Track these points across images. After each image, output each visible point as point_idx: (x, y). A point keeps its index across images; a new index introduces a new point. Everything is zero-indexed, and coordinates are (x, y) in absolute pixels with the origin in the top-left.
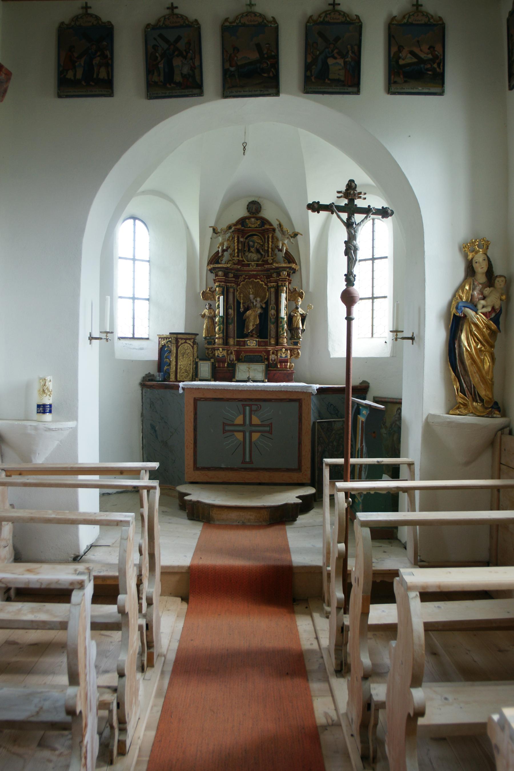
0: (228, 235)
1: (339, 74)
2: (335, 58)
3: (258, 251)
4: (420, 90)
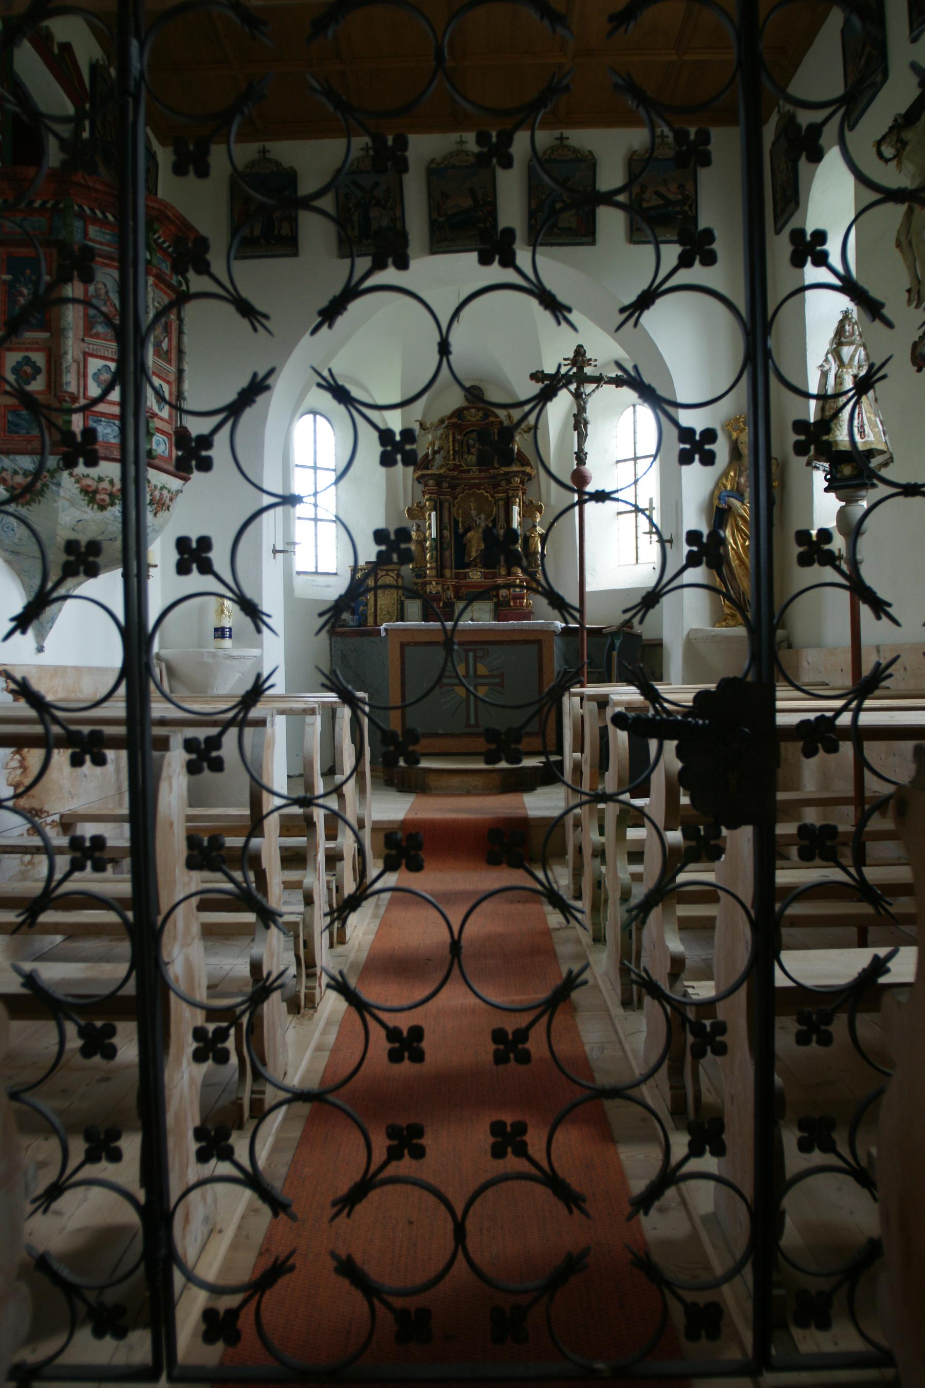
0: (440, 432)
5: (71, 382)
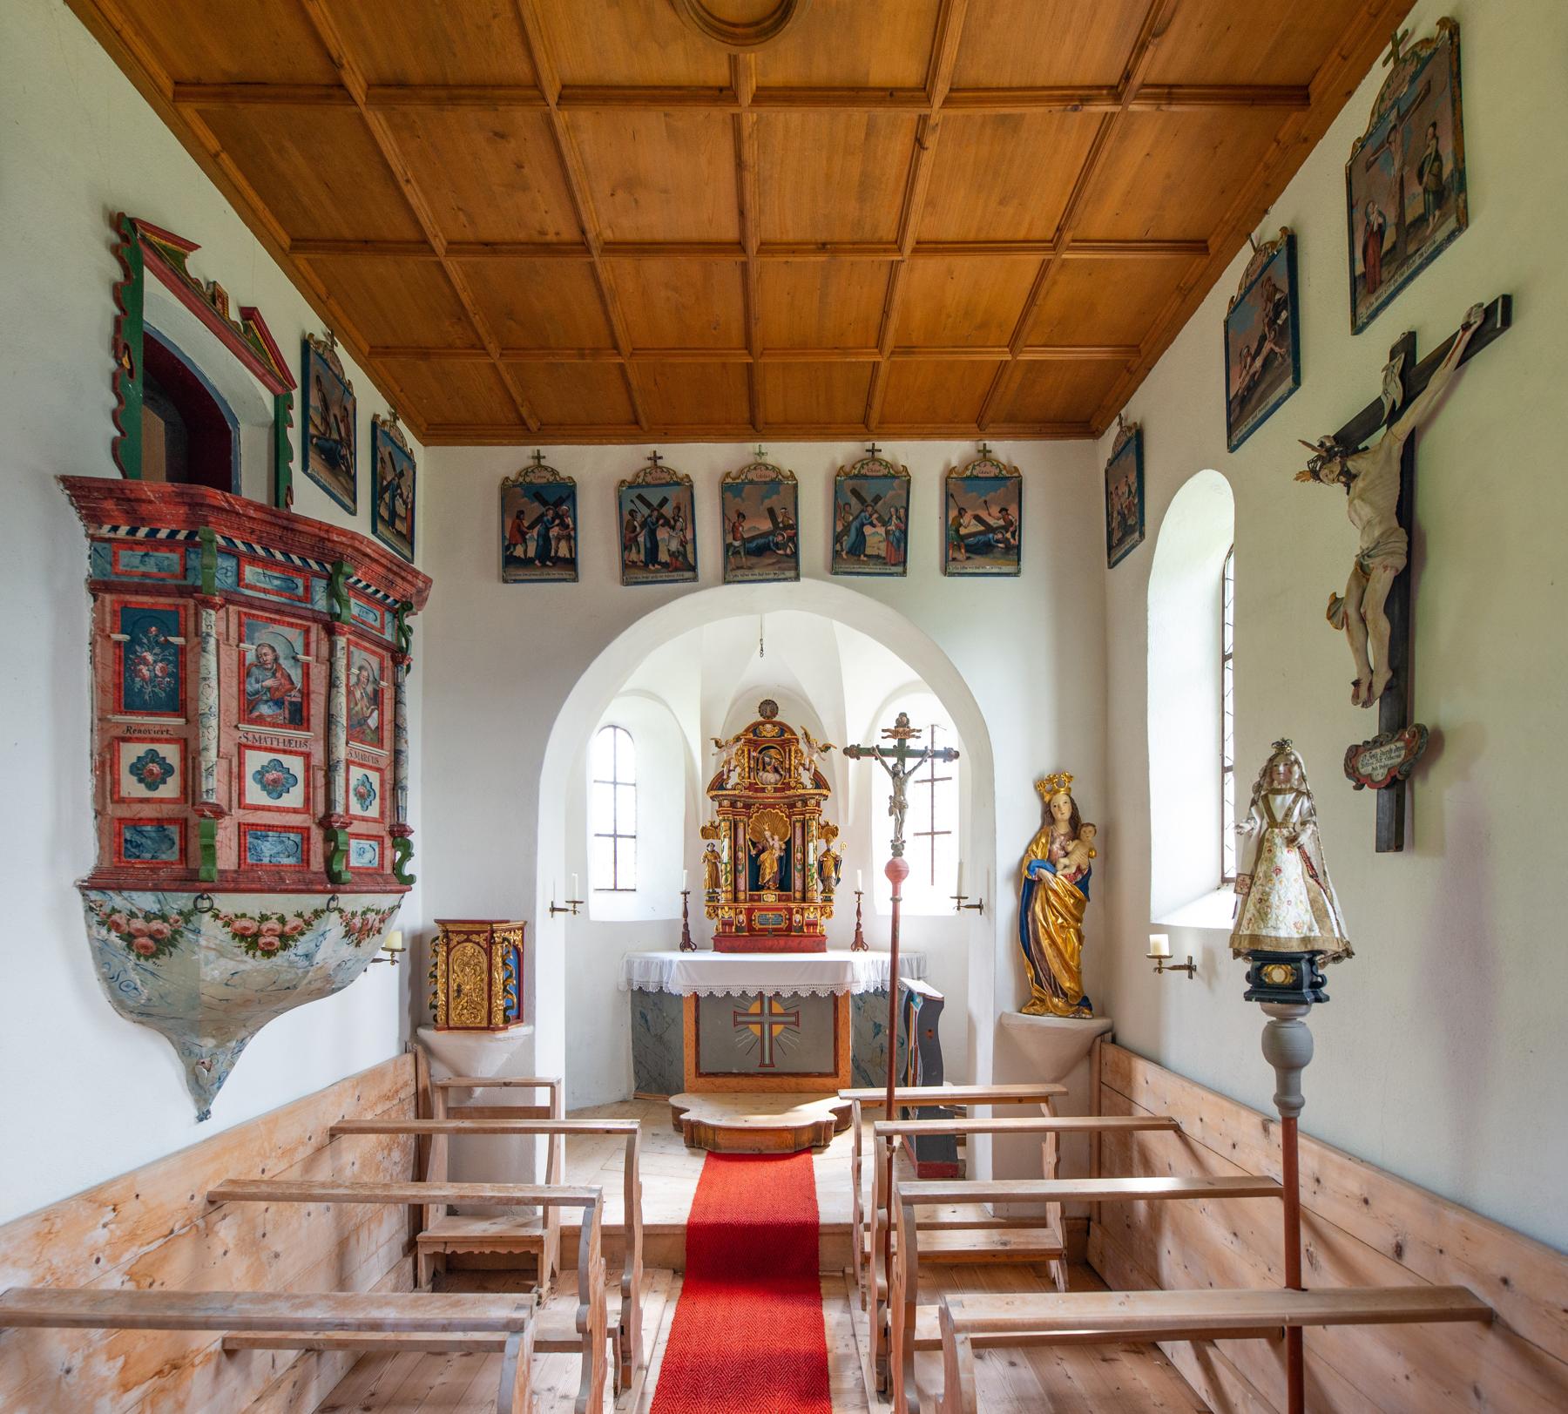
3: (776, 770)
4: (988, 569)
5: (214, 787)
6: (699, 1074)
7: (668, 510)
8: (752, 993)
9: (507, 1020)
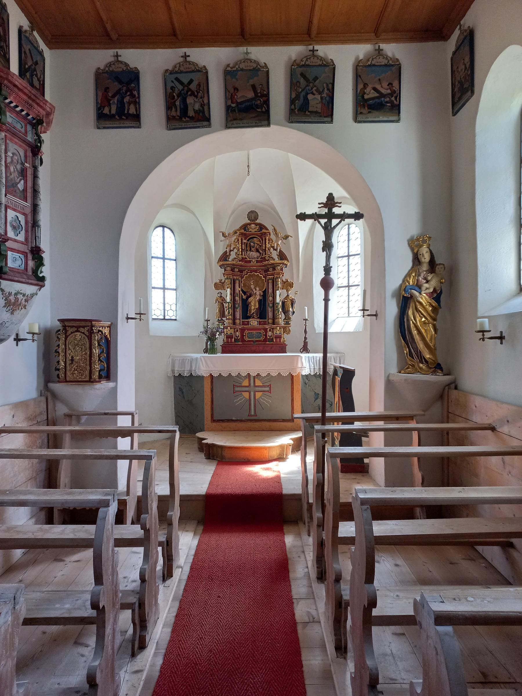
0: (233, 239)
1: (317, 107)
2: (314, 94)
3: (257, 251)
4: (381, 118)
6: (213, 421)
7: (193, 86)
8: (244, 374)
9: (100, 377)
